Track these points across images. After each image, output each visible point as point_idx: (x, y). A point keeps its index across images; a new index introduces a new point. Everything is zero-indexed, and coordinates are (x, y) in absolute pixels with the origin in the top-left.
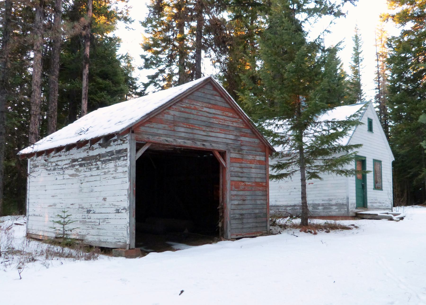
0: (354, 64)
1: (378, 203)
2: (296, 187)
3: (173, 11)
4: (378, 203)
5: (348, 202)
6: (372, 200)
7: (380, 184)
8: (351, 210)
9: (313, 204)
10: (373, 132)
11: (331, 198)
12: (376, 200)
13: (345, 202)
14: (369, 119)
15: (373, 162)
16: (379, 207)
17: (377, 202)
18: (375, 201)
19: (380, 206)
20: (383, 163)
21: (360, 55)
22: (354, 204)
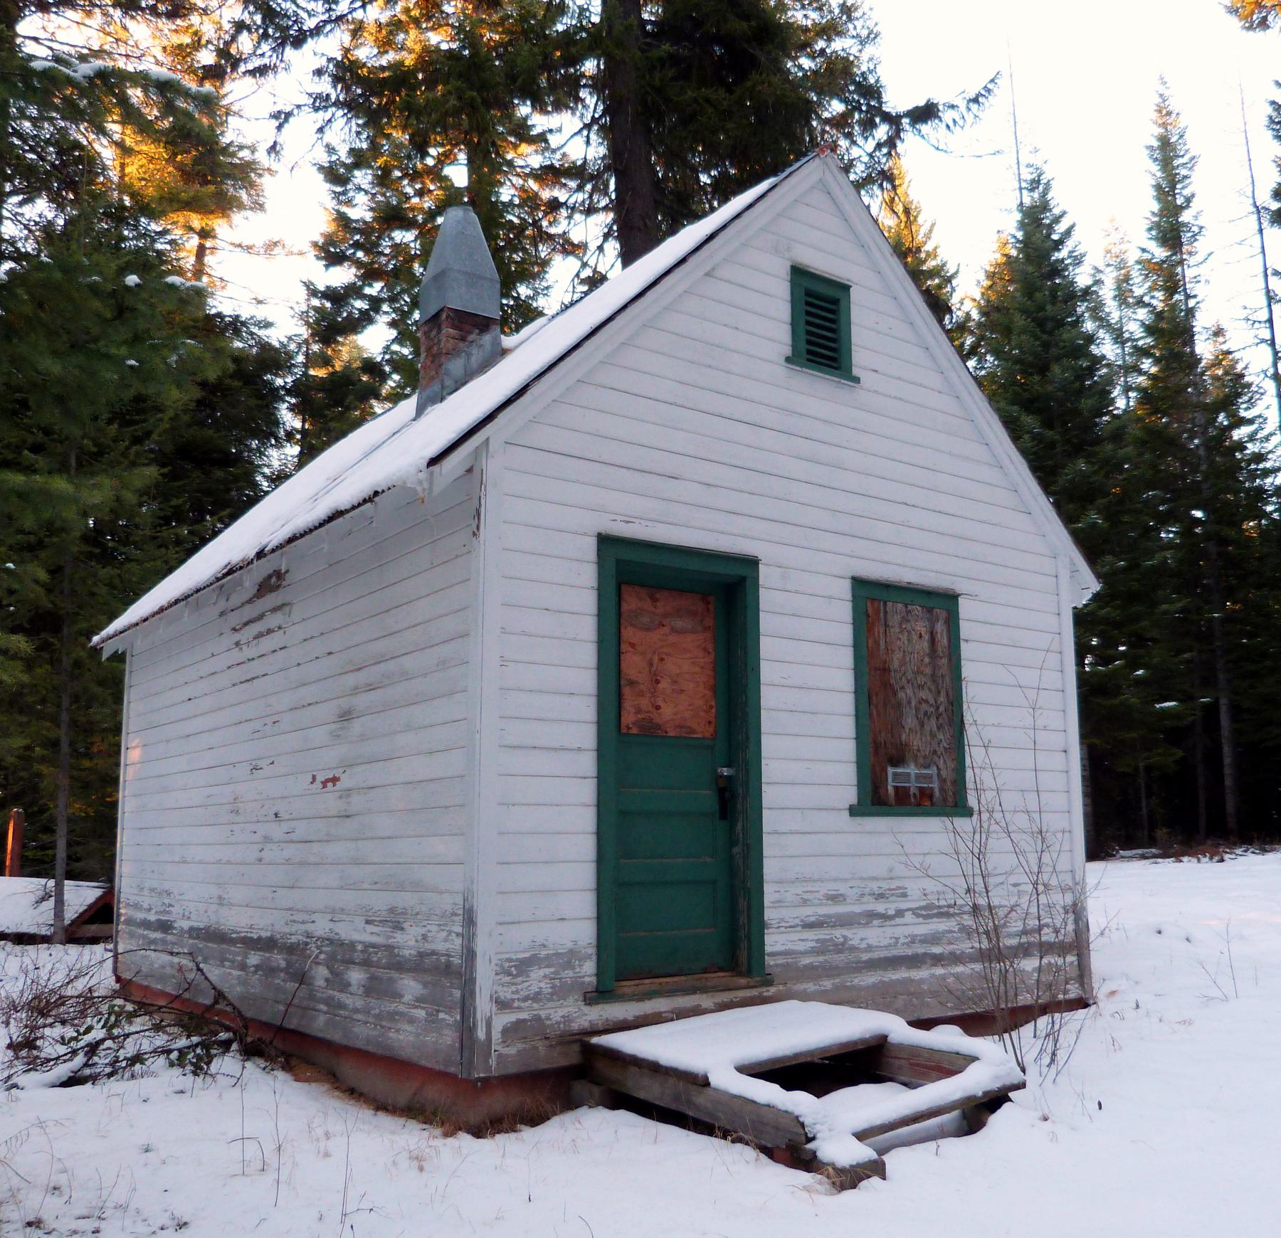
0: (1160, 253)
1: (909, 917)
2: (281, 807)
3: (448, 171)
4: (909, 917)
5: (470, 955)
6: (835, 898)
7: (946, 766)
8: (502, 1020)
9: (332, 941)
10: (856, 371)
11: (406, 900)
12: (880, 896)
13: (447, 943)
14: (799, 273)
15: (855, 598)
16: (920, 949)
17: (900, 913)
18: (880, 907)
19: (934, 939)
20: (966, 608)
21: (1185, 217)
22: (570, 958)
